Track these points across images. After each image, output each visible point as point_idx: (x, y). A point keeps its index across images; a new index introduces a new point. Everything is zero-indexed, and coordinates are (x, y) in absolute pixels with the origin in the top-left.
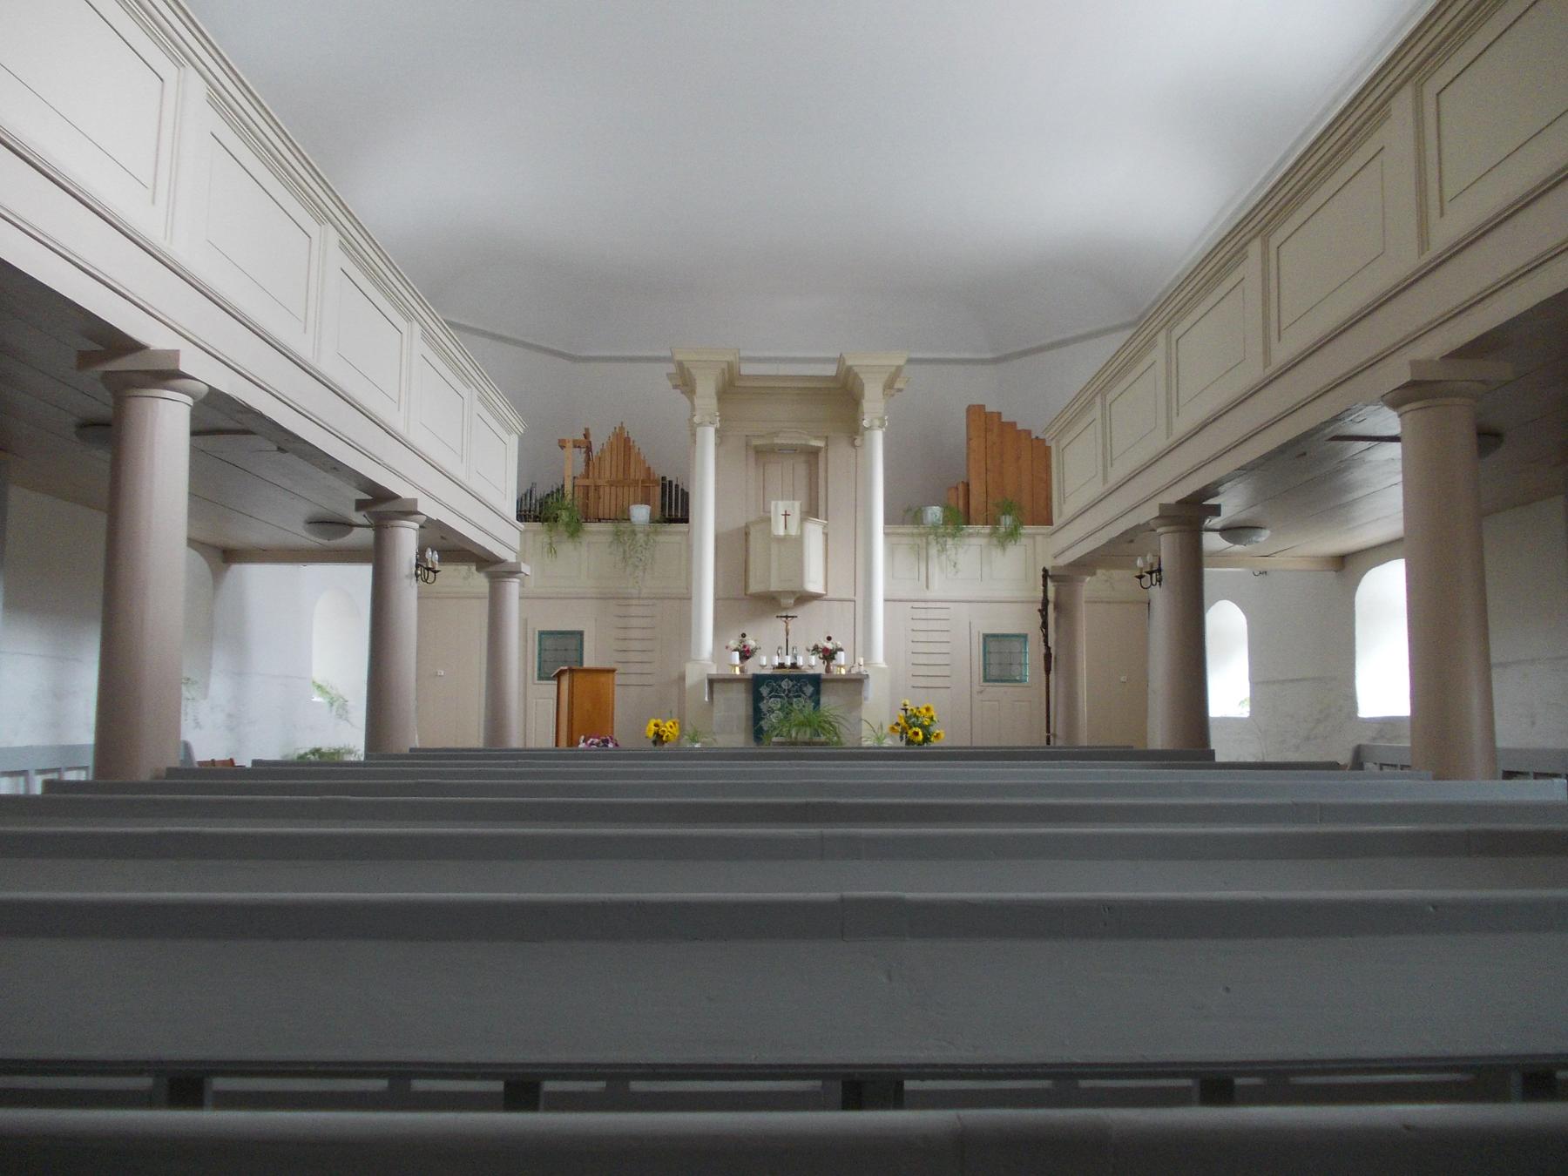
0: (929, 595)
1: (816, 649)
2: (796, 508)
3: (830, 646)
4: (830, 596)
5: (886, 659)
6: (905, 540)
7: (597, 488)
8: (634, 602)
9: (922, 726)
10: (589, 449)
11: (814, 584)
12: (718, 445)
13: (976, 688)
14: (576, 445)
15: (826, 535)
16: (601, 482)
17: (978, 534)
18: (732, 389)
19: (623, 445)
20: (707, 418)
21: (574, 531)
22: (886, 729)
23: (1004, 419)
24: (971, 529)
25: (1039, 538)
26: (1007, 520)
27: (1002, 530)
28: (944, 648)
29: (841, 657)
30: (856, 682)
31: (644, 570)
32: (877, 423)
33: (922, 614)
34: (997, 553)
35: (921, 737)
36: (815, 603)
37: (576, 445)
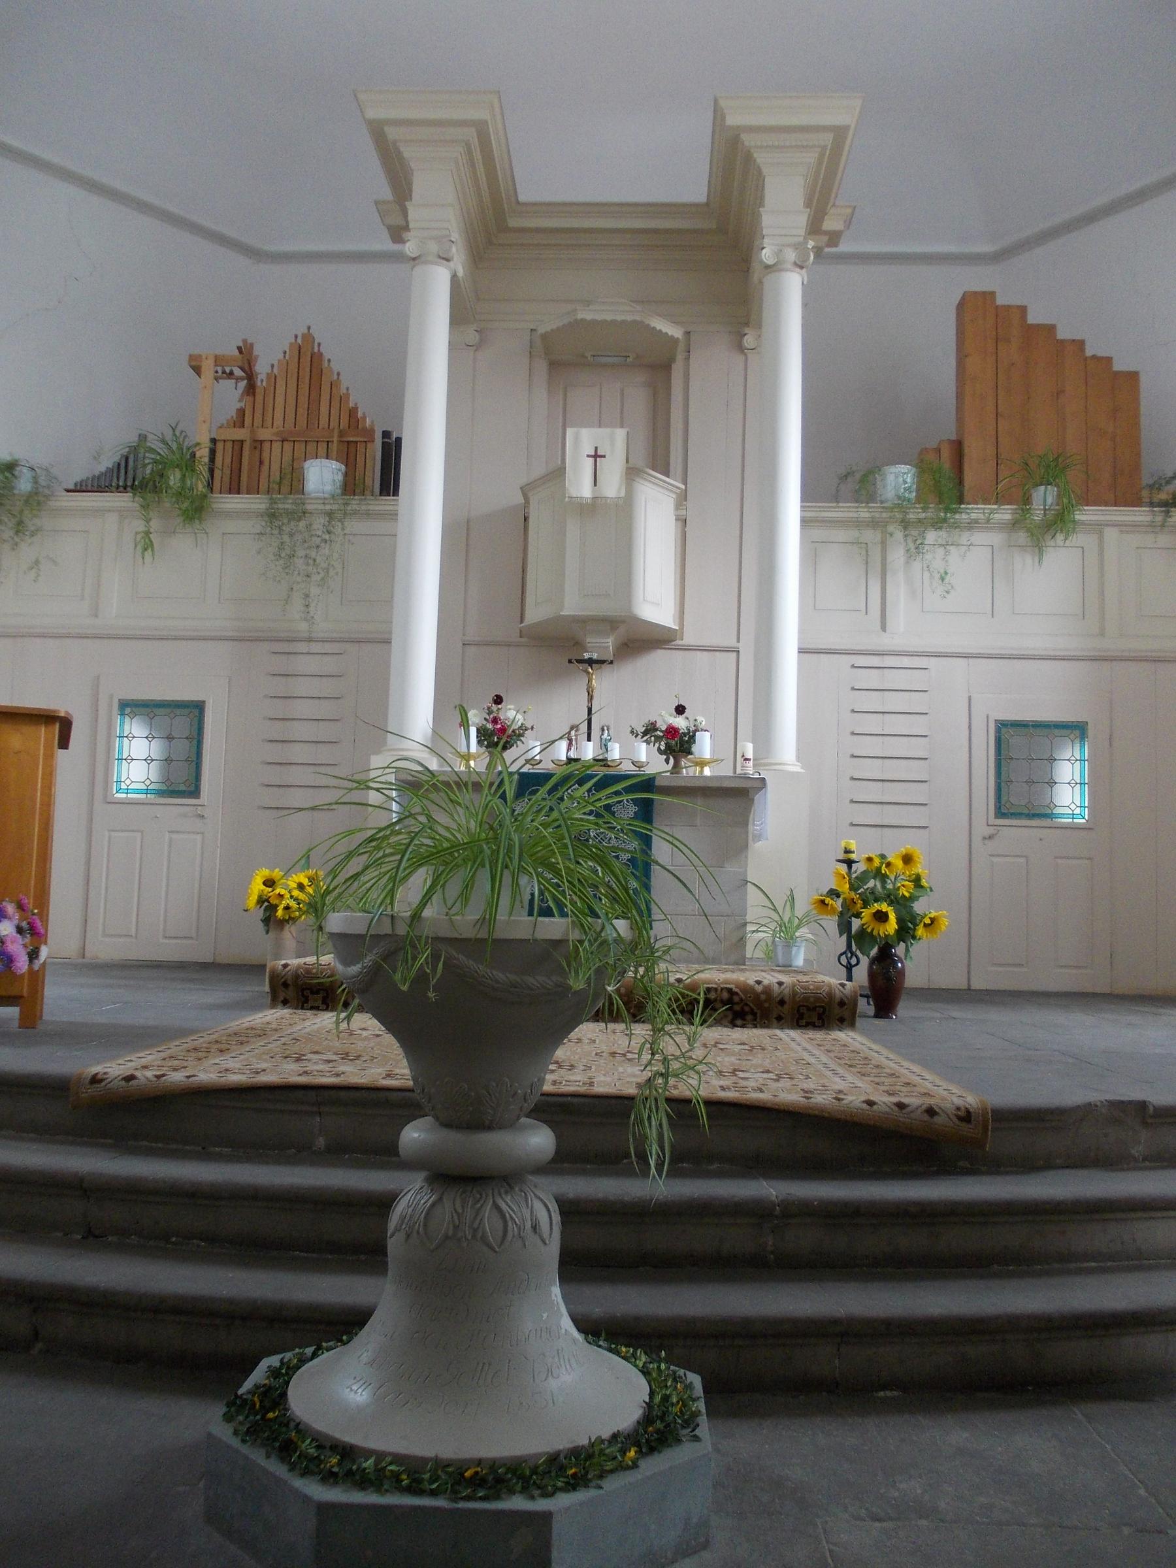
0: (886, 641)
1: (650, 730)
3: (680, 723)
4: (689, 639)
5: (798, 759)
6: (841, 535)
7: (258, 444)
8: (302, 647)
9: (893, 898)
10: (250, 377)
11: (655, 604)
13: (981, 829)
15: (683, 521)
16: (264, 434)
17: (987, 525)
18: (502, 235)
19: (308, 361)
20: (433, 247)
21: (195, 511)
22: (803, 906)
23: (1031, 319)
24: (975, 511)
25: (1111, 534)
26: (1044, 497)
27: (1037, 516)
28: (917, 748)
29: (704, 746)
30: (737, 796)
31: (322, 583)
32: (791, 255)
33: (872, 679)
34: (1024, 562)
35: (892, 926)
36: (659, 657)
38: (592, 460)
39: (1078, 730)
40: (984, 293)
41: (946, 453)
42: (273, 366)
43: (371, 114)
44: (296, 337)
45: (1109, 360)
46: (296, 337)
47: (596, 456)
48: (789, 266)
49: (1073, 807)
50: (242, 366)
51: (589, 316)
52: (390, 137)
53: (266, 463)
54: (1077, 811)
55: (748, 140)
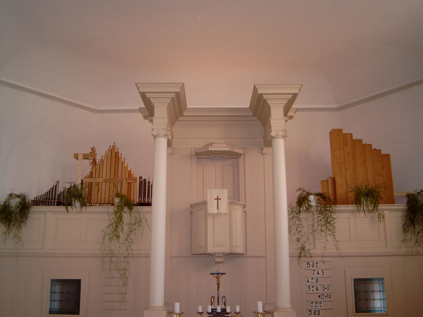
2: (224, 194)
4: (249, 254)
12: (170, 155)
14: (86, 157)
16: (100, 180)
19: (114, 155)
23: (354, 138)
37: (86, 157)
38: (216, 200)
39: (381, 280)
40: (339, 129)
41: (330, 182)
42: (102, 156)
43: (142, 90)
44: (110, 146)
45: (380, 150)
46: (110, 146)
47: (218, 199)
48: (281, 137)
49: (381, 307)
50: (91, 156)
51: (213, 149)
52: (147, 96)
53: (100, 190)
54: (383, 309)
55: (265, 97)
